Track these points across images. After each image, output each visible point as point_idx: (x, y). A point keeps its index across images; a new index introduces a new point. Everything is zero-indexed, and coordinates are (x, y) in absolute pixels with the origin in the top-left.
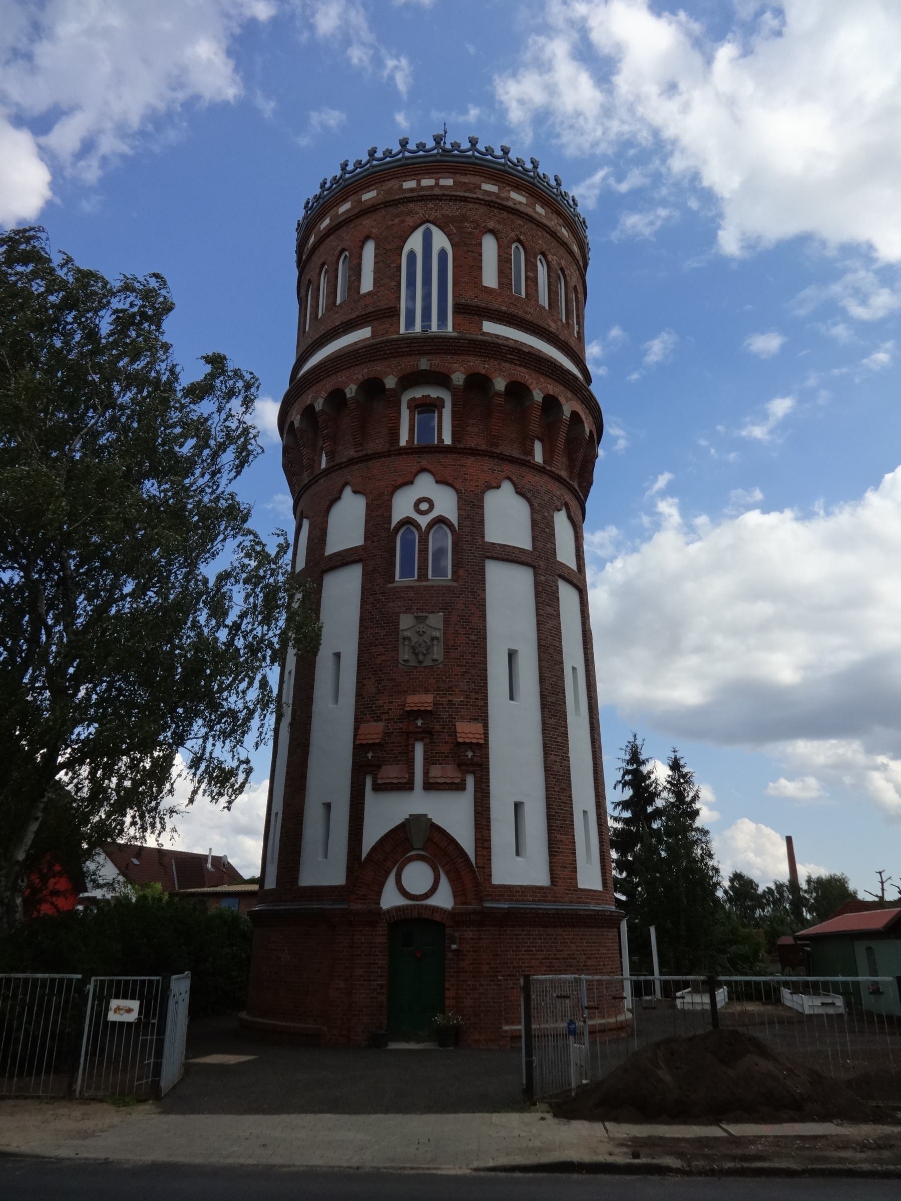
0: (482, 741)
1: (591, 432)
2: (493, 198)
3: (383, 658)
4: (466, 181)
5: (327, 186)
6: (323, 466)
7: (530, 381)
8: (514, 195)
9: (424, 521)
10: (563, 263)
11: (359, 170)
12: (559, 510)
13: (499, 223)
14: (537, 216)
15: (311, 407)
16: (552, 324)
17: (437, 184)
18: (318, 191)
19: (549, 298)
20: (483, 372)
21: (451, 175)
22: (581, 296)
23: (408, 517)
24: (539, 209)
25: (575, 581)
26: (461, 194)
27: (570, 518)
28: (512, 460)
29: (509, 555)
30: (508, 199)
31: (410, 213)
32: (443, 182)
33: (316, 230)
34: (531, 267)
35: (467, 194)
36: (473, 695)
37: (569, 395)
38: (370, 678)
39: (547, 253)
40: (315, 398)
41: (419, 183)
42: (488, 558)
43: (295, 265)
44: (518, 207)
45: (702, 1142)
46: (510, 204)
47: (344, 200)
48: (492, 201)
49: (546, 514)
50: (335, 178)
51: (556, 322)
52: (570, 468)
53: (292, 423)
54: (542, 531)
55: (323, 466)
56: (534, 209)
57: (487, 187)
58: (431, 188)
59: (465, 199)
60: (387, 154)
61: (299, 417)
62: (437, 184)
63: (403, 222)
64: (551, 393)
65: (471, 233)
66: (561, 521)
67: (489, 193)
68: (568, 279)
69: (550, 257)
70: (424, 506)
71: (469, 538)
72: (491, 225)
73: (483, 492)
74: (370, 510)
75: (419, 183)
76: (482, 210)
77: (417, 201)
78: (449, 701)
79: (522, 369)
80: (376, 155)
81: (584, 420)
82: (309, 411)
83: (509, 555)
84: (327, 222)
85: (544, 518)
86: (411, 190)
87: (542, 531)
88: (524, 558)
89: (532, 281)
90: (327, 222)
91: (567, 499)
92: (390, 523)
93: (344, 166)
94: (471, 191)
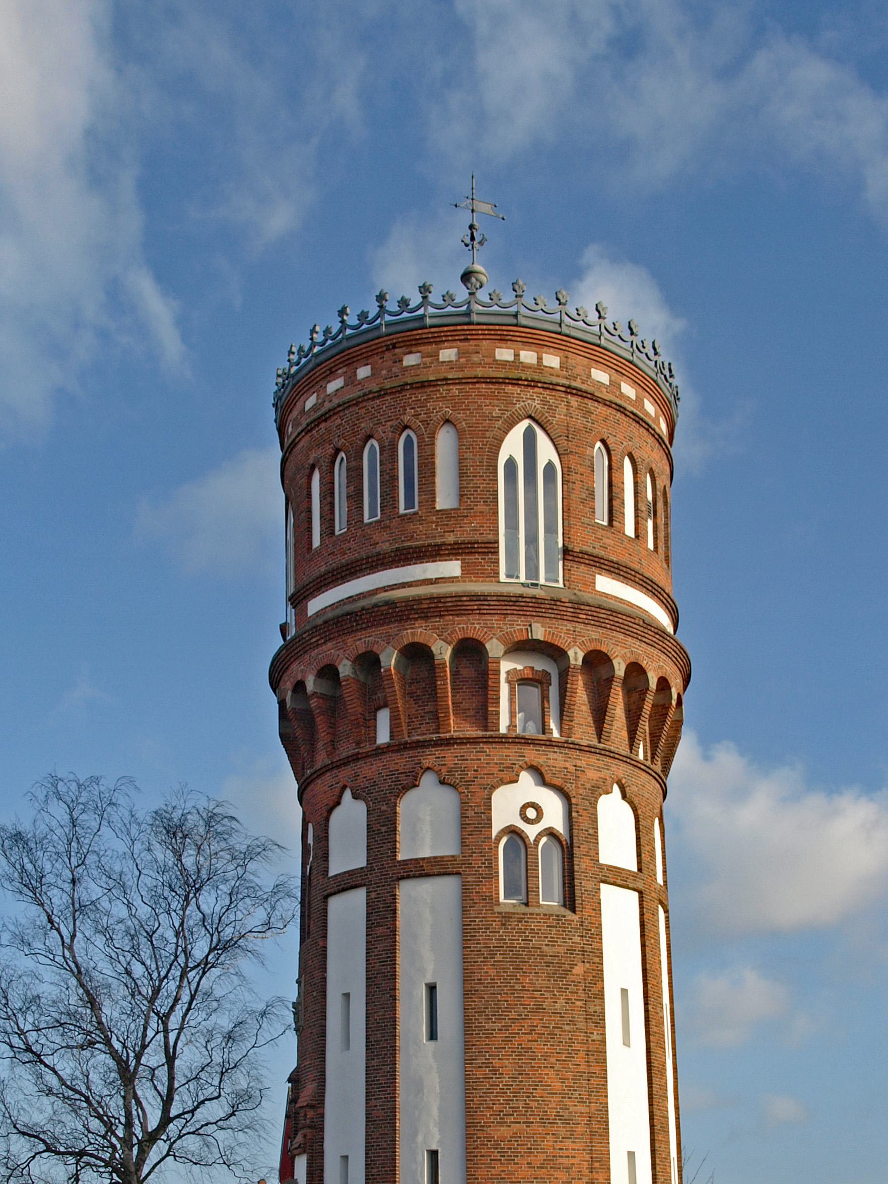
9: (531, 831)
70: (531, 813)
83: (617, 877)
86: (505, 364)
92: (490, 826)
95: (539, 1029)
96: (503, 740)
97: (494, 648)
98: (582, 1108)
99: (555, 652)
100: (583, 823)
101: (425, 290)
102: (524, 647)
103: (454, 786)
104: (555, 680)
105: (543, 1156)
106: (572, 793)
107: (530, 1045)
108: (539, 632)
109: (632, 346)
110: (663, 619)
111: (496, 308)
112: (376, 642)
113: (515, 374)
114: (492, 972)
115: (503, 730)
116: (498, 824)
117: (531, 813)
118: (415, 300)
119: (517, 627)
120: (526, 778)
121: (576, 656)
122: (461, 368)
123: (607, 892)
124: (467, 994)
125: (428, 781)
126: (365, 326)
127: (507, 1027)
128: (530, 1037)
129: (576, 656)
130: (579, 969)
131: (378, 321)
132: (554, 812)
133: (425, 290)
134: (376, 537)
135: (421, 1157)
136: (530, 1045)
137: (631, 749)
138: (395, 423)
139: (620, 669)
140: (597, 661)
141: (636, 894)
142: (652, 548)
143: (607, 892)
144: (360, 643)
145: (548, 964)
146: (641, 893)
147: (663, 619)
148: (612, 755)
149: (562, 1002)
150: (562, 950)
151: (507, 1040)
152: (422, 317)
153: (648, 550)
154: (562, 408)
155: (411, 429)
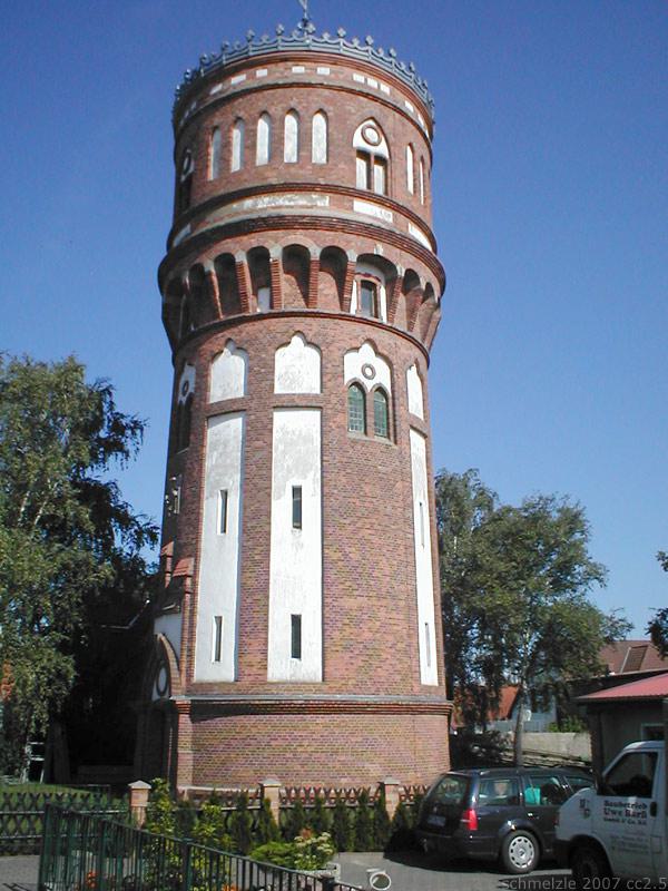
9: (369, 385)
70: (368, 372)
86: (359, 84)
95: (376, 527)
98: (402, 587)
100: (399, 382)
103: (316, 346)
105: (378, 623)
106: (394, 362)
107: (370, 537)
110: (428, 245)
112: (265, 242)
113: (366, 91)
114: (344, 480)
116: (348, 377)
117: (368, 372)
120: (367, 348)
122: (331, 80)
125: (297, 341)
127: (354, 523)
128: (369, 532)
129: (401, 271)
130: (399, 485)
132: (383, 377)
134: (268, 174)
135: (208, 643)
136: (370, 537)
137: (306, 296)
138: (285, 105)
142: (412, 192)
144: (253, 241)
145: (381, 479)
147: (428, 245)
149: (389, 508)
150: (390, 469)
151: (354, 532)
153: (407, 192)
154: (391, 119)
155: (386, 169)
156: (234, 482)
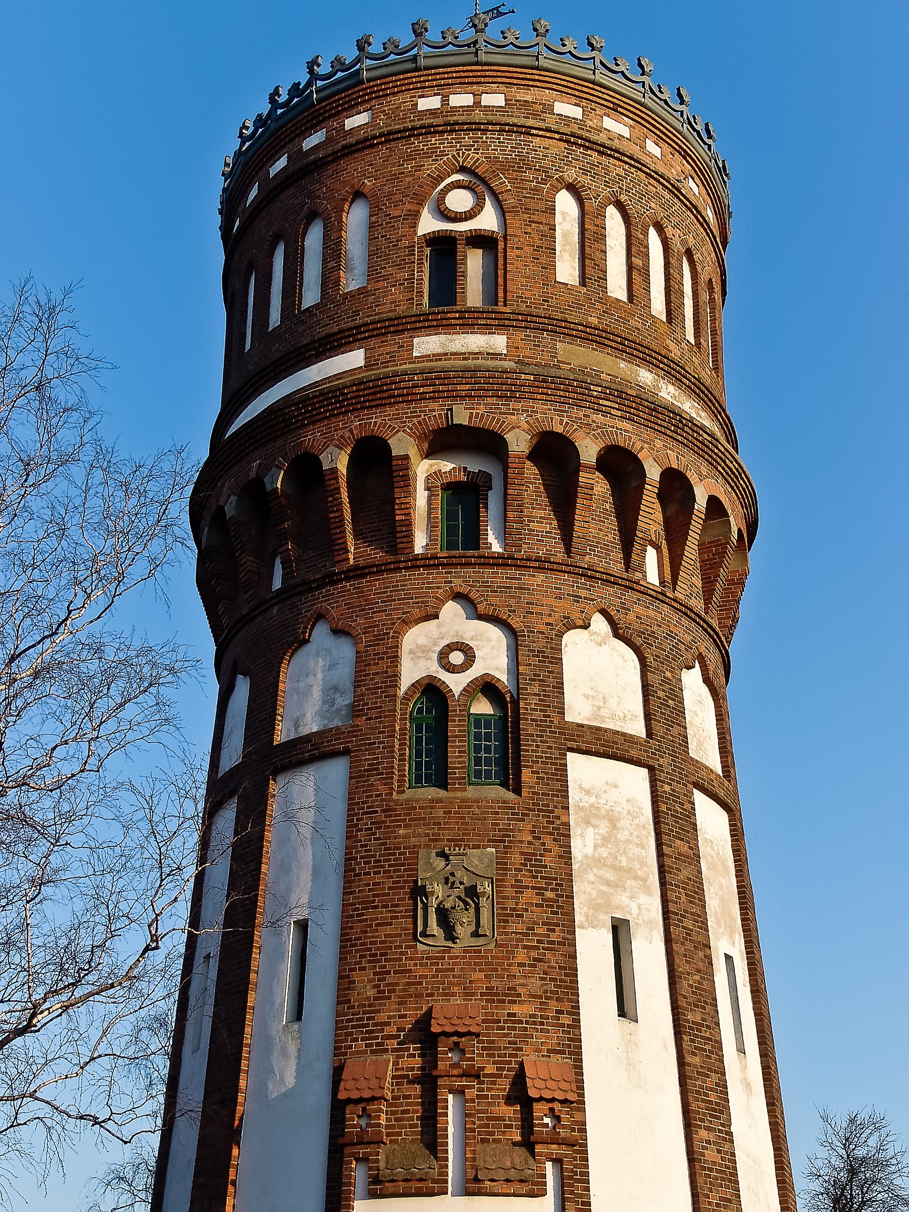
0: (572, 1097)
1: (740, 531)
2: (575, 128)
3: (389, 930)
4: (529, 98)
5: (282, 99)
6: (277, 584)
7: (638, 445)
8: (609, 123)
9: (456, 683)
10: (691, 242)
11: (340, 74)
12: (689, 668)
13: (585, 172)
14: (648, 160)
15: (258, 483)
16: (672, 345)
17: (477, 104)
18: (265, 108)
19: (668, 302)
20: (559, 429)
21: (502, 88)
22: (717, 296)
23: (430, 677)
24: (652, 147)
25: (721, 794)
26: (522, 121)
27: (707, 681)
28: (609, 580)
29: (606, 745)
30: (600, 130)
31: (432, 152)
32: (488, 100)
33: (261, 175)
34: (635, 248)
35: (530, 122)
36: (553, 1005)
37: (704, 469)
38: (364, 969)
39: (665, 223)
40: (265, 469)
41: (445, 101)
42: (572, 750)
43: (216, 187)
44: (616, 144)
45: (420, 293)
46: (602, 138)
47: (312, 128)
48: (573, 135)
49: (668, 674)
50: (296, 86)
51: (678, 343)
52: (708, 593)
53: (221, 509)
54: (662, 704)
55: (277, 584)
56: (643, 148)
57: (564, 108)
58: (467, 109)
59: (527, 131)
60: (391, 48)
61: (233, 499)
62: (477, 104)
63: (419, 168)
64: (675, 466)
65: (536, 189)
66: (692, 682)
67: (567, 120)
68: (699, 268)
69: (669, 231)
70: (457, 658)
71: (538, 715)
72: (571, 175)
73: (560, 635)
74: (361, 663)
75: (445, 101)
76: (557, 148)
77: (442, 133)
78: (509, 1015)
79: (626, 425)
80: (371, 50)
81: (730, 512)
82: (255, 491)
83: (606, 745)
84: (282, 162)
85: (666, 681)
86: (432, 113)
87: (662, 704)
88: (633, 753)
89: (636, 271)
90: (282, 162)
91: (702, 650)
92: (396, 685)
93: (312, 65)
94: (535, 115)
96: (417, 563)
97: (402, 444)
99: (490, 443)
101: (418, 30)
102: (443, 441)
104: (497, 483)
108: (462, 416)
109: (643, 87)
111: (392, 57)
115: (418, 550)
118: (406, 38)
119: (433, 413)
120: (451, 610)
121: (519, 442)
123: (582, 770)
124: (346, 942)
126: (340, 74)
129: (519, 442)
131: (358, 67)
132: (493, 654)
133: (418, 30)
139: (653, 473)
140: (554, 453)
141: (644, 772)
143: (582, 770)
146: (651, 769)
148: (590, 575)
152: (414, 59)
156: (645, 909)
